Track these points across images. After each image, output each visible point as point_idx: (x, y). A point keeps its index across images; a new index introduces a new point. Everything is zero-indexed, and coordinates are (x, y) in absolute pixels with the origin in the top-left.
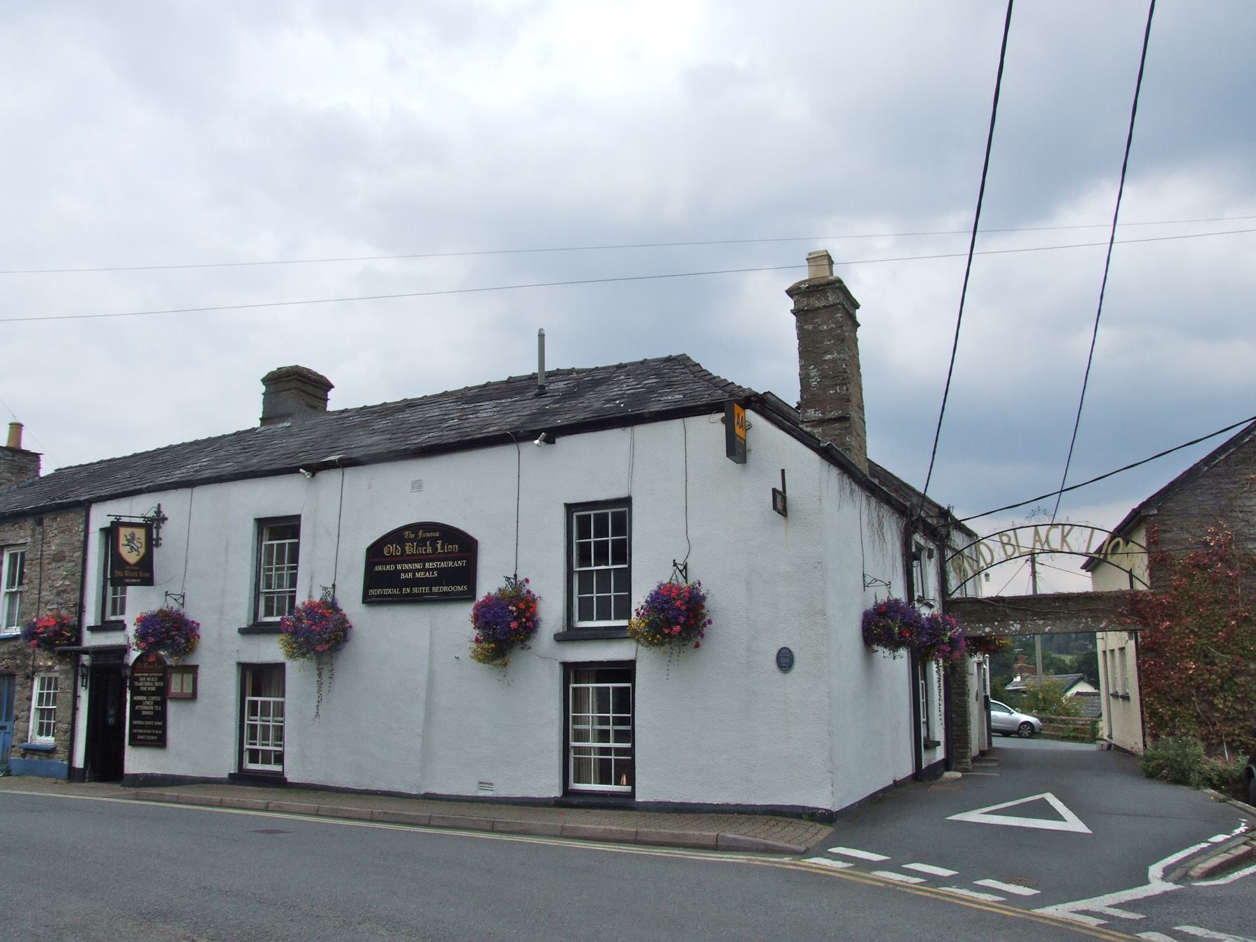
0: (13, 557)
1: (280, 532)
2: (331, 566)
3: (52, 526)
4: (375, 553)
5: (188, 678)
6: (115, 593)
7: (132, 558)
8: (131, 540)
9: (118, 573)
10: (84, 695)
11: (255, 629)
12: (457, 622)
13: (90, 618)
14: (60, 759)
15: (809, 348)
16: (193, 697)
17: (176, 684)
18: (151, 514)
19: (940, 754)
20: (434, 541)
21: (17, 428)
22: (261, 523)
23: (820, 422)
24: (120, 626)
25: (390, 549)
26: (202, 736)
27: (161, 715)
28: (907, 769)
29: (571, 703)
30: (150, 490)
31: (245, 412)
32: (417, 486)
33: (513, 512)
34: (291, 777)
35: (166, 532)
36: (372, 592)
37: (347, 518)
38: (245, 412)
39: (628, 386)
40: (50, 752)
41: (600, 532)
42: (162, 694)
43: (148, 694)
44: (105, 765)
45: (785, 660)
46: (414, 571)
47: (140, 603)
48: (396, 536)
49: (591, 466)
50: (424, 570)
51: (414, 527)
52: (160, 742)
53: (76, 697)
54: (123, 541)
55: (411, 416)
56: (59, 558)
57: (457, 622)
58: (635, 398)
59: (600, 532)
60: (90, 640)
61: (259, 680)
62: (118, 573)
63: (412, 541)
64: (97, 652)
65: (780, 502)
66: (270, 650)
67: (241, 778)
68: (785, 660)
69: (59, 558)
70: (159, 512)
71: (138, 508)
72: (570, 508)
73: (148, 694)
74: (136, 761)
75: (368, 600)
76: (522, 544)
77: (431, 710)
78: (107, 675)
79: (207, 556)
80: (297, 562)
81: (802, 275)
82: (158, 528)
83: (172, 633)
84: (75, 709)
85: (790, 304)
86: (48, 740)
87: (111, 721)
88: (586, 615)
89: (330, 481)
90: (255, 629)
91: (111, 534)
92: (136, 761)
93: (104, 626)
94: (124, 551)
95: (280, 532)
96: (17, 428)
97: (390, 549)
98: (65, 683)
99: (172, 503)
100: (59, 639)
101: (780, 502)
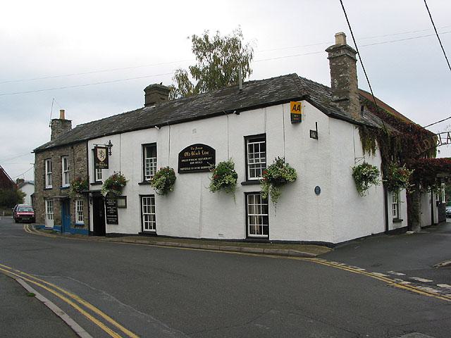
0: (48, 162)
1: (150, 150)
2: (168, 158)
3: (77, 148)
4: (181, 155)
5: (123, 200)
6: (98, 171)
7: (102, 159)
8: (101, 153)
9: (97, 164)
10: (91, 207)
11: (144, 183)
12: (206, 179)
13: (91, 181)
14: (86, 228)
15: (335, 72)
16: (125, 207)
17: (121, 202)
18: (108, 144)
19: (405, 224)
20: (201, 151)
21: (62, 112)
22: (246, 138)
23: (336, 101)
24: (100, 183)
25: (187, 154)
26: (129, 221)
27: (116, 213)
28: (383, 230)
29: (248, 209)
30: (107, 135)
31: (138, 102)
32: (194, 131)
33: (225, 137)
34: (158, 234)
35: (113, 149)
36: (182, 169)
37: (172, 142)
38: (138, 102)
39: (272, 89)
40: (82, 226)
41: (256, 144)
42: (116, 206)
43: (112, 206)
44: (99, 230)
45: (318, 191)
46: (195, 161)
47: (106, 175)
48: (188, 149)
49: (252, 122)
50: (198, 161)
51: (194, 146)
52: (116, 223)
53: (89, 208)
54: (98, 153)
55: (365, 95)
56: (79, 160)
57: (206, 179)
58: (272, 95)
59: (256, 144)
60: (93, 188)
61: (147, 201)
62: (97, 164)
63: (193, 151)
64: (94, 192)
65: (314, 135)
66: (149, 190)
67: (142, 234)
68: (318, 191)
69: (79, 160)
70: (110, 143)
71: (103, 142)
72: (246, 138)
73: (112, 206)
74: (109, 229)
75: (180, 172)
76: (230, 150)
77: (199, 213)
78: (97, 199)
79: (125, 155)
80: (265, 150)
81: (332, 42)
82: (110, 149)
83: (117, 184)
84: (89, 212)
85: (327, 54)
86: (82, 222)
87: (101, 215)
88: (253, 176)
89: (166, 130)
90: (144, 183)
91: (95, 150)
92: (109, 229)
93: (96, 183)
94: (99, 157)
95: (150, 150)
96: (62, 112)
97: (187, 154)
98: (85, 203)
99: (114, 139)
100: (82, 187)
101: (314, 135)
